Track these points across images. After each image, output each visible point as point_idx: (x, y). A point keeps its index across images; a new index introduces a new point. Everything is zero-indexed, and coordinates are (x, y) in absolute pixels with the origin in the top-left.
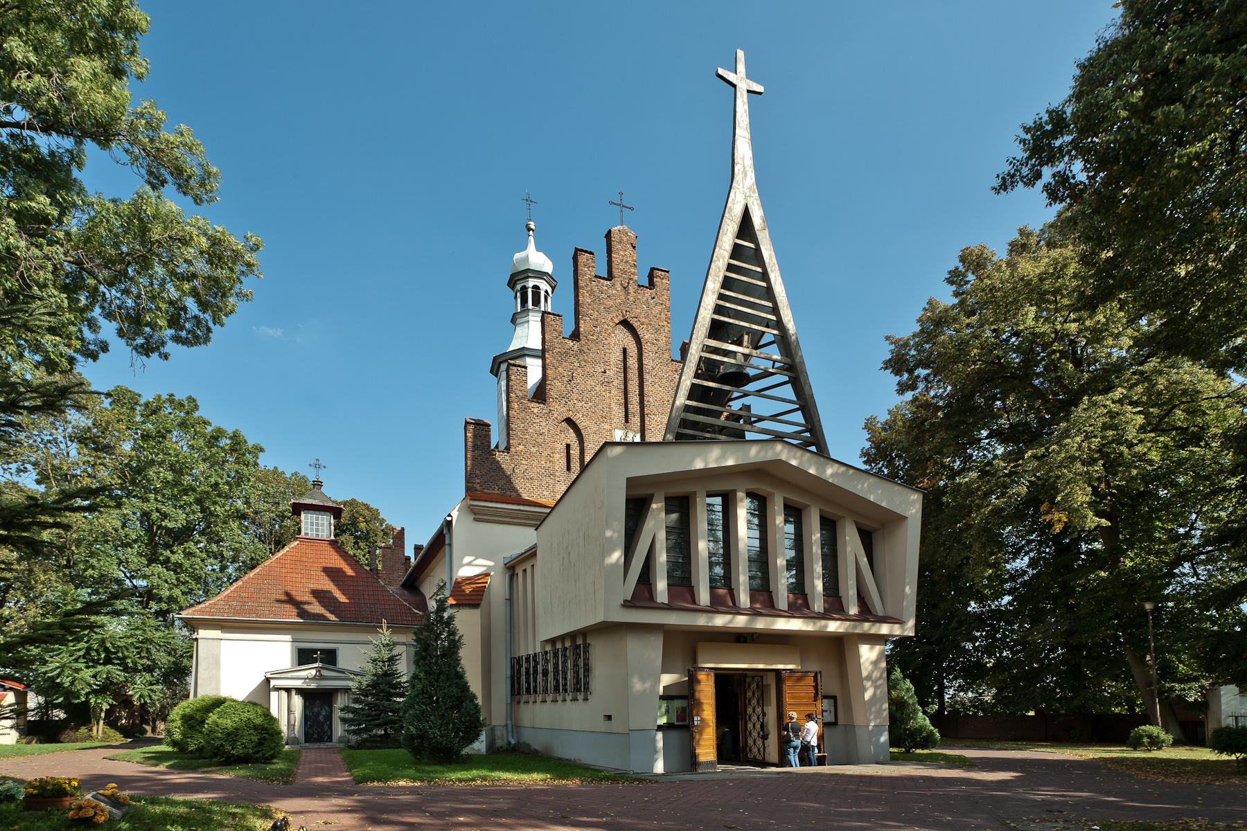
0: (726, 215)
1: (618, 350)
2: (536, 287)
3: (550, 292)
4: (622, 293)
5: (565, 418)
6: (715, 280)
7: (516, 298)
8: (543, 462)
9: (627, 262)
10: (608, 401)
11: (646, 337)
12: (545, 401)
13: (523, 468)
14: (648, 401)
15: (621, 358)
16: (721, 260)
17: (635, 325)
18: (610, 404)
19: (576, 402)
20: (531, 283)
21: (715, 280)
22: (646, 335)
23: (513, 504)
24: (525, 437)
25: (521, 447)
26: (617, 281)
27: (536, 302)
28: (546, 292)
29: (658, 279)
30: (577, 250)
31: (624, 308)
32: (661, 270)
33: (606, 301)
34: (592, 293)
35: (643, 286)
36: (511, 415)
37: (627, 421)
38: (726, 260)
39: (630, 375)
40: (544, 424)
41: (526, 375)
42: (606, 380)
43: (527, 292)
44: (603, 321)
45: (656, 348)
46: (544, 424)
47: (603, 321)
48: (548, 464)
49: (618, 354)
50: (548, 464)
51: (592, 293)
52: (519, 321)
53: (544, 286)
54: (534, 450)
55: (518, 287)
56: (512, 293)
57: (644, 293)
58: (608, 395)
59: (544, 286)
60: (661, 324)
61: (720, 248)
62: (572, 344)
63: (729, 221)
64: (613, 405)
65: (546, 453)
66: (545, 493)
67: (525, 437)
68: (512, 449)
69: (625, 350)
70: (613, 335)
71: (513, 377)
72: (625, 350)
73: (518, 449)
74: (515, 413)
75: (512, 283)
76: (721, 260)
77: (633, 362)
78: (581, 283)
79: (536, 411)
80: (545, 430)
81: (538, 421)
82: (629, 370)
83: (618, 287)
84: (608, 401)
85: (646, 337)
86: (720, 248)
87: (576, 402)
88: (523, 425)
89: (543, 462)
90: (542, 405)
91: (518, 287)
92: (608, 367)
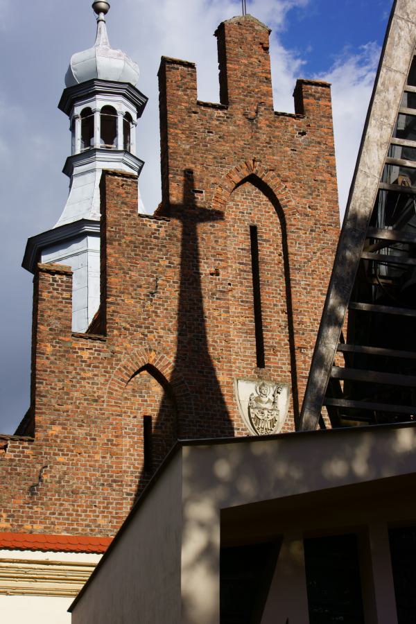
0: (397, 12)
1: (242, 231)
2: (109, 111)
3: (134, 116)
4: (246, 130)
5: (141, 365)
6: (382, 124)
7: (73, 128)
8: (98, 457)
9: (253, 75)
10: (223, 327)
11: (293, 203)
12: (105, 335)
13: (58, 470)
14: (301, 323)
15: (247, 244)
16: (391, 89)
17: (272, 183)
18: (227, 334)
19: (162, 333)
20: (98, 103)
21: (382, 124)
22: (291, 199)
23: (11, 549)
24: (64, 407)
25: (56, 429)
26: (237, 109)
27: (109, 136)
28: (128, 116)
29: (311, 100)
30: (165, 62)
31: (250, 155)
32: (317, 84)
33: (217, 147)
34: (191, 133)
35: (283, 114)
36: (38, 366)
37: (261, 363)
38: (400, 89)
39: (264, 276)
40: (102, 380)
41: (69, 288)
42: (220, 288)
43: (92, 118)
44: (212, 180)
45: (312, 223)
46: (102, 380)
47: (212, 180)
48: (109, 461)
49: (241, 238)
50: (109, 461)
51: (191, 133)
52: (77, 170)
53: (122, 106)
54: (80, 432)
55: (78, 110)
56: (65, 119)
57: (286, 126)
58: (224, 316)
59: (122, 106)
60: (320, 178)
61: (389, 69)
62: (155, 226)
63: (402, 23)
64: (233, 333)
65: (102, 439)
66: (101, 521)
67: (64, 407)
68: (39, 435)
69: (254, 231)
70: (231, 204)
71: (45, 295)
72: (254, 231)
73: (50, 432)
74: (47, 362)
75: (66, 104)
76: (391, 89)
77: (270, 252)
78: (171, 118)
79: (86, 355)
80: (103, 393)
81: (90, 374)
82: (262, 267)
83: (239, 117)
84: (223, 327)
85: (293, 203)
86: (389, 69)
87: (162, 333)
88: (60, 385)
89: (98, 457)
90: (97, 344)
91: (78, 110)
92: (222, 264)
